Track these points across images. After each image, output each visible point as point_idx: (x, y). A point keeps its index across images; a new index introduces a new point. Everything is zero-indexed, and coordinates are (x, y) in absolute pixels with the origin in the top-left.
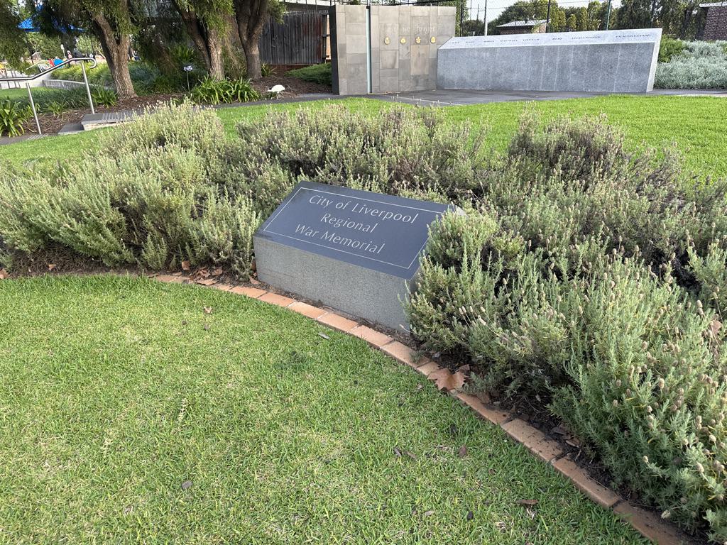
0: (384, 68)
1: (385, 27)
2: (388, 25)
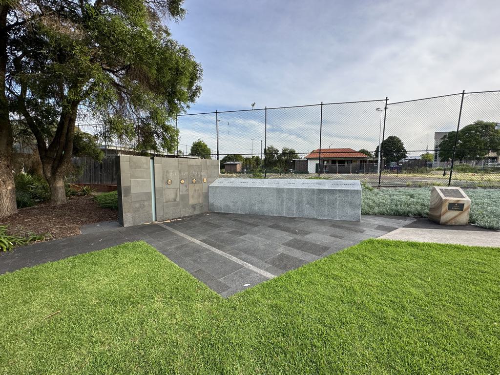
0: (167, 202)
1: (167, 172)
2: (170, 171)
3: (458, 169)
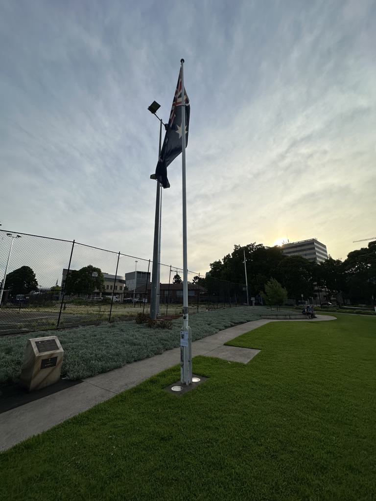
3: (76, 302)
